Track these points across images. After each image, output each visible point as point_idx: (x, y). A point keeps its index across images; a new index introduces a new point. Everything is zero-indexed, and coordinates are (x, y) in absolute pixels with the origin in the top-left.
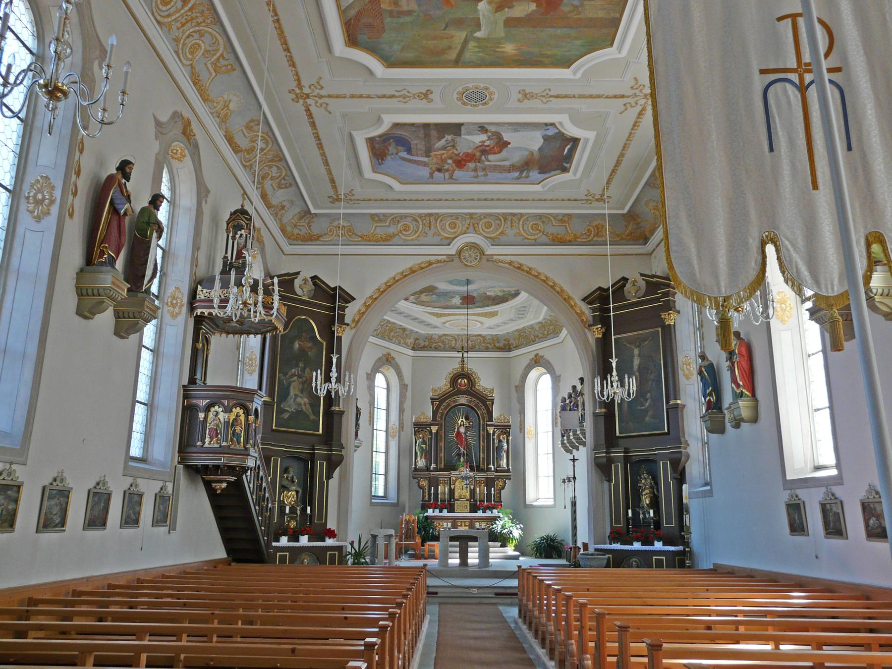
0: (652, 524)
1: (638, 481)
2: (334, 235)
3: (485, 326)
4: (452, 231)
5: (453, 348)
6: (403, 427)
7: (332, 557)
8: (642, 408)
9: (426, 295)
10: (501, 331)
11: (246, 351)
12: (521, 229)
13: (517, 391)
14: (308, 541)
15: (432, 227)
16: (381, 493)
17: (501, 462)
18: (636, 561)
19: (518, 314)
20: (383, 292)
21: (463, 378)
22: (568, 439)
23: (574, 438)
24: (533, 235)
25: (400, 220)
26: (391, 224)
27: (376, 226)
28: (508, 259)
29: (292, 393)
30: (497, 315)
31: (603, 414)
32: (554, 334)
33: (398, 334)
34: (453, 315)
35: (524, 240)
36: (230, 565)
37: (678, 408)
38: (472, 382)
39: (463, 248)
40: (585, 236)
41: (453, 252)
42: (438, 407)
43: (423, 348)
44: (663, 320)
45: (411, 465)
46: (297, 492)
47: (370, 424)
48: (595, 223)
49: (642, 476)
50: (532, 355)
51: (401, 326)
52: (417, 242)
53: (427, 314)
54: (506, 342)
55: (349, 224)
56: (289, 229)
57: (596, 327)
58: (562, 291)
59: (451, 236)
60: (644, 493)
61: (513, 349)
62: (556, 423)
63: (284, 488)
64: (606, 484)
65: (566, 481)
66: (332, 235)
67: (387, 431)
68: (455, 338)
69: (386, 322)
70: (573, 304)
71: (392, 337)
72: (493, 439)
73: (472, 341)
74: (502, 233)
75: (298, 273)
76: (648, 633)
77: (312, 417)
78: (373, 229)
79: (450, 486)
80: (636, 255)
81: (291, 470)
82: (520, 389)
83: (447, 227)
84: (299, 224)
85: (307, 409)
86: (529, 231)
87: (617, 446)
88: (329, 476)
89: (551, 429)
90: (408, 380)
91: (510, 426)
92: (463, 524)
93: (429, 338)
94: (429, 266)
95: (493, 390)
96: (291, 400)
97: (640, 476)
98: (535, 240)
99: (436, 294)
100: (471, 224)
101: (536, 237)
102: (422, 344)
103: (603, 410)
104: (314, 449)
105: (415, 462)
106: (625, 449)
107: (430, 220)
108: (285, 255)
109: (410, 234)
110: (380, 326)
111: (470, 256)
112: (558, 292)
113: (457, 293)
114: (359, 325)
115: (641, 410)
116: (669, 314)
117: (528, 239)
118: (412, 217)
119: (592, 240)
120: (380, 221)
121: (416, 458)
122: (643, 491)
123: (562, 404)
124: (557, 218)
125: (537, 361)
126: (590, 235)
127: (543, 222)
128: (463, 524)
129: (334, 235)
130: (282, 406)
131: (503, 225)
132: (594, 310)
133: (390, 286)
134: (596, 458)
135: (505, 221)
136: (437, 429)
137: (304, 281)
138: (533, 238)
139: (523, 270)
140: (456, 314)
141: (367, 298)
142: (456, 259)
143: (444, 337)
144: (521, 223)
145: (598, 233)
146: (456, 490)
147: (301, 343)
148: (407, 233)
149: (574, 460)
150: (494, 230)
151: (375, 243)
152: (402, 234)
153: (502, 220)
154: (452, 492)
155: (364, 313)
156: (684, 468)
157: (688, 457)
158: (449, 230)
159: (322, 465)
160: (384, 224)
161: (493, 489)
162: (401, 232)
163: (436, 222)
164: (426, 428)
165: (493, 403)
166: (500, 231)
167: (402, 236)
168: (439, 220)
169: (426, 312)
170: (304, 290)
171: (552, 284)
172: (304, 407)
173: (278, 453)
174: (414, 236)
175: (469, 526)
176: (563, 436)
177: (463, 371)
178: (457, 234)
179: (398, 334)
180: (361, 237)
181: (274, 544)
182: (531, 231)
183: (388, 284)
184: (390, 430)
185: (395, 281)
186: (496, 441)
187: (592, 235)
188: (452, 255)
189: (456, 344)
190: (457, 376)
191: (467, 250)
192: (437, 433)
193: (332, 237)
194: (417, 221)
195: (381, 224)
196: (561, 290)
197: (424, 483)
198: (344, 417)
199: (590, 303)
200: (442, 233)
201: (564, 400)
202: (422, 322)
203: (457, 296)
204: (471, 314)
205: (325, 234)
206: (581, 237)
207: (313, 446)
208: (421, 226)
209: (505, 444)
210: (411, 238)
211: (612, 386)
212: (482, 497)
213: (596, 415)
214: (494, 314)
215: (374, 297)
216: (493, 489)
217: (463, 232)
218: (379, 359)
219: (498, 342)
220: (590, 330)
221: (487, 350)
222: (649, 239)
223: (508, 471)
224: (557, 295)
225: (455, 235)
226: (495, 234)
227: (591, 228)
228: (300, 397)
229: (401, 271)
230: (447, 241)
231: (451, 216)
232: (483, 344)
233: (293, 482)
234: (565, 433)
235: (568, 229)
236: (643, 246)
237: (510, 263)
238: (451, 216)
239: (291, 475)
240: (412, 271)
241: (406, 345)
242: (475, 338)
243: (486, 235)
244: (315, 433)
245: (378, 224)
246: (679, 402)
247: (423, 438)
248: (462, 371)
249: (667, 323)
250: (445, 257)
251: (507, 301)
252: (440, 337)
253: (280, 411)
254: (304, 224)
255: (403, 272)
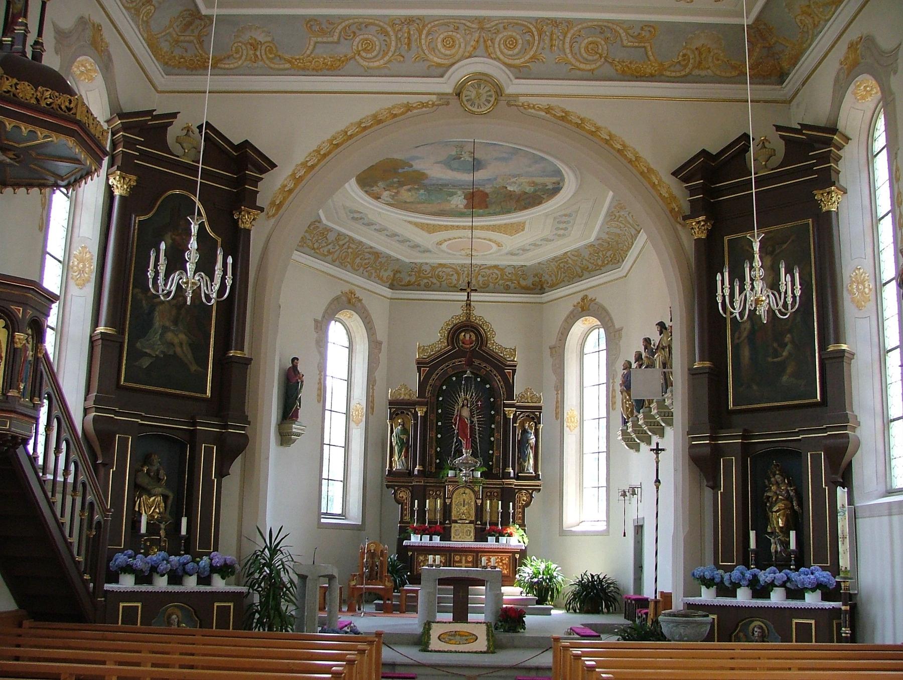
0: (793, 562)
1: (766, 488)
2: (244, 57)
3: (505, 250)
4: (448, 52)
5: (455, 286)
6: (373, 408)
7: (224, 611)
8: (775, 360)
9: (409, 190)
10: (530, 260)
11: (74, 245)
12: (568, 51)
13: (552, 355)
14: (136, 584)
15: (414, 45)
16: (337, 509)
17: (526, 464)
18: (760, 627)
19: (557, 229)
20: (325, 155)
21: (466, 331)
22: (635, 425)
23: (646, 423)
24: (587, 61)
25: (357, 31)
26: (342, 40)
27: (316, 43)
28: (544, 102)
29: (158, 322)
30: (523, 230)
31: (707, 371)
32: (614, 263)
33: (367, 261)
34: (452, 227)
35: (573, 72)
36: (20, 625)
37: (843, 357)
38: (481, 337)
39: (467, 81)
40: (678, 67)
41: (448, 89)
42: (428, 376)
43: (408, 286)
44: (817, 205)
45: (384, 466)
46: (165, 498)
47: (319, 401)
48: (697, 43)
49: (773, 479)
50: (578, 299)
51: (371, 247)
52: (386, 71)
53: (410, 226)
54: (537, 279)
55: (269, 39)
56: (165, 46)
57: (697, 220)
58: (638, 158)
59: (446, 62)
60: (775, 509)
61: (547, 289)
62: (614, 403)
63: (138, 489)
64: (708, 493)
65: (627, 494)
66: (240, 58)
67: (348, 414)
68: (457, 270)
69: (347, 239)
70: (656, 183)
71: (358, 266)
72: (514, 428)
73: (483, 276)
74: (534, 58)
75: (174, 115)
76: (660, 673)
77: (194, 368)
78: (311, 47)
79: (445, 500)
80: (766, 102)
81: (156, 459)
82: (558, 352)
83: (440, 46)
84: (182, 38)
85: (185, 353)
86: (581, 55)
87: (729, 427)
88: (222, 473)
89: (604, 413)
90: (382, 335)
91: (540, 408)
92: (464, 558)
93: (417, 270)
94: (407, 112)
95: (515, 350)
96: (155, 337)
97: (769, 479)
98: (592, 70)
99: (425, 187)
100: (482, 40)
101: (593, 66)
102: (407, 279)
103: (707, 364)
104: (194, 424)
105: (391, 462)
106: (745, 430)
107: (409, 32)
108: (158, 92)
109: (374, 57)
110: (337, 247)
111: (478, 96)
112: (630, 161)
113: (456, 185)
114: (281, 212)
115: (774, 363)
116: (828, 193)
117: (579, 69)
118: (380, 26)
119: (690, 73)
120: (323, 32)
121: (391, 456)
122: (773, 504)
123: (625, 372)
124: (630, 31)
125: (585, 307)
126: (685, 66)
127: (606, 39)
128: (464, 558)
129: (244, 57)
130: (138, 345)
131: (536, 42)
132: (692, 191)
133: (338, 145)
134: (692, 447)
135: (540, 35)
136: (425, 410)
137: (185, 132)
138: (588, 67)
139: (570, 122)
140: (458, 227)
141: (297, 165)
142: (454, 101)
143: (440, 269)
144: (568, 40)
145: (700, 63)
146: (453, 506)
147: (177, 238)
148: (369, 56)
149: (657, 450)
150: (520, 52)
151: (315, 73)
152: (362, 57)
153: (535, 33)
154: (447, 510)
155: (291, 191)
156: (850, 464)
157: (858, 445)
158: (443, 50)
159: (209, 451)
160: (330, 39)
161: (511, 504)
162: (359, 54)
163: (420, 36)
164: (408, 409)
165: (514, 371)
166: (532, 53)
167: (361, 61)
168: (425, 32)
169: (410, 222)
170: (184, 145)
171: (620, 147)
172: (178, 350)
173: (127, 428)
174: (382, 62)
175: (472, 562)
176: (625, 422)
177: (468, 315)
178: (457, 58)
179: (367, 261)
180: (290, 62)
181: (107, 587)
182: (585, 55)
183: (334, 142)
184: (353, 413)
185: (347, 137)
186: (519, 432)
187: (690, 66)
188: (447, 94)
189: (458, 280)
190: (457, 330)
191: (472, 85)
192: (424, 418)
193: (240, 63)
194: (387, 34)
195: (325, 40)
196: (636, 157)
197: (404, 495)
198: (252, 366)
199: (685, 180)
200: (431, 57)
201: (628, 366)
202: (404, 241)
203: (459, 192)
204: (482, 228)
205: (228, 57)
206: (672, 68)
207: (193, 418)
208: (393, 43)
209: (533, 436)
210: (377, 64)
211: (753, 288)
212: (494, 519)
213: (693, 374)
214: (518, 228)
215: (309, 164)
216: (511, 504)
217: (467, 54)
218: (337, 299)
219: (524, 279)
220: (684, 226)
221: (507, 290)
222: (788, 74)
223: (537, 478)
224: (629, 166)
225: (452, 61)
226: (523, 60)
227: (689, 53)
228: (173, 331)
229: (358, 120)
230: (440, 70)
231: (447, 24)
232: (501, 282)
233: (159, 480)
234: (628, 418)
235: (650, 53)
236: (778, 87)
237: (548, 110)
238: (447, 24)
239: (155, 468)
240: (377, 120)
241: (381, 280)
242: (488, 272)
243: (506, 60)
244: (199, 395)
245: (319, 39)
246: (844, 347)
247: (403, 425)
248: (467, 320)
249: (824, 209)
250: (434, 98)
251: (540, 203)
252: (433, 268)
253: (135, 354)
254: (192, 38)
255: (360, 123)
